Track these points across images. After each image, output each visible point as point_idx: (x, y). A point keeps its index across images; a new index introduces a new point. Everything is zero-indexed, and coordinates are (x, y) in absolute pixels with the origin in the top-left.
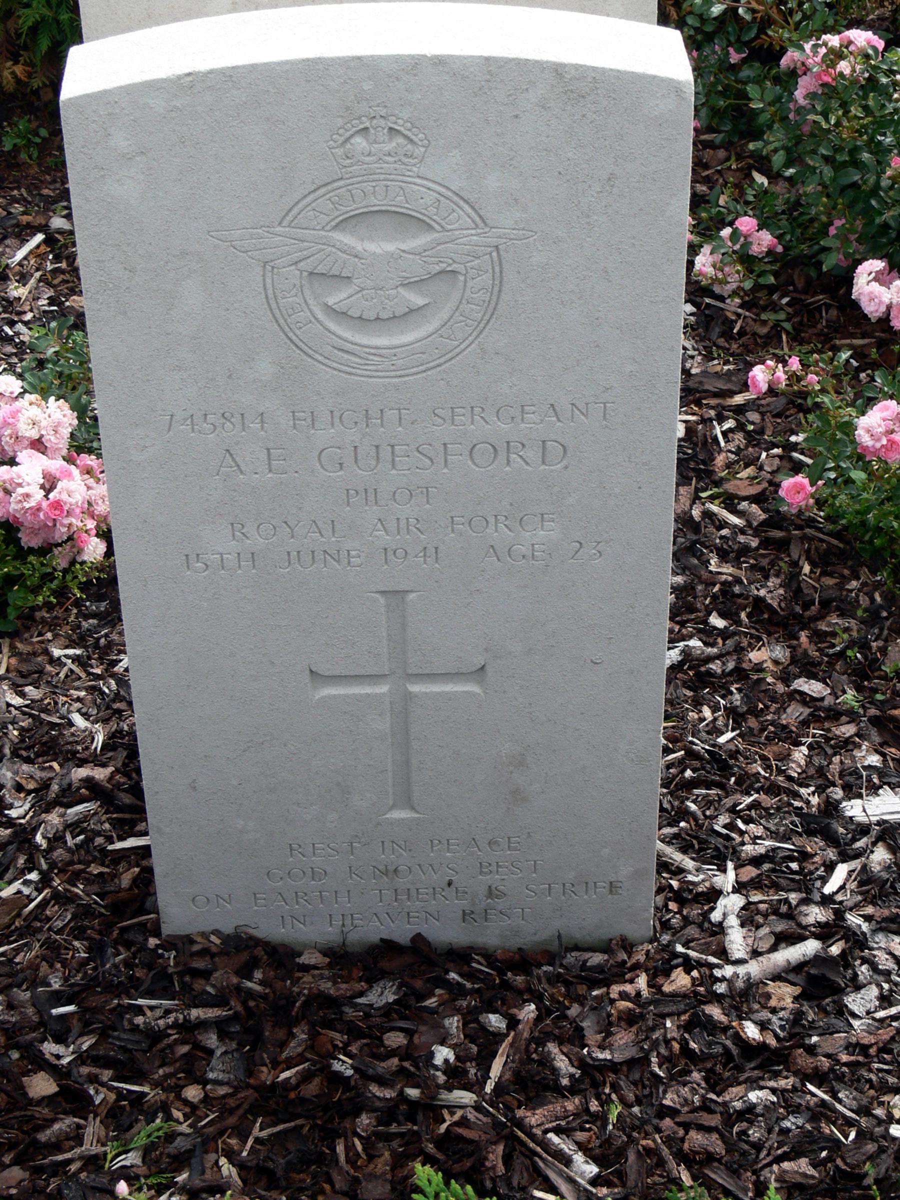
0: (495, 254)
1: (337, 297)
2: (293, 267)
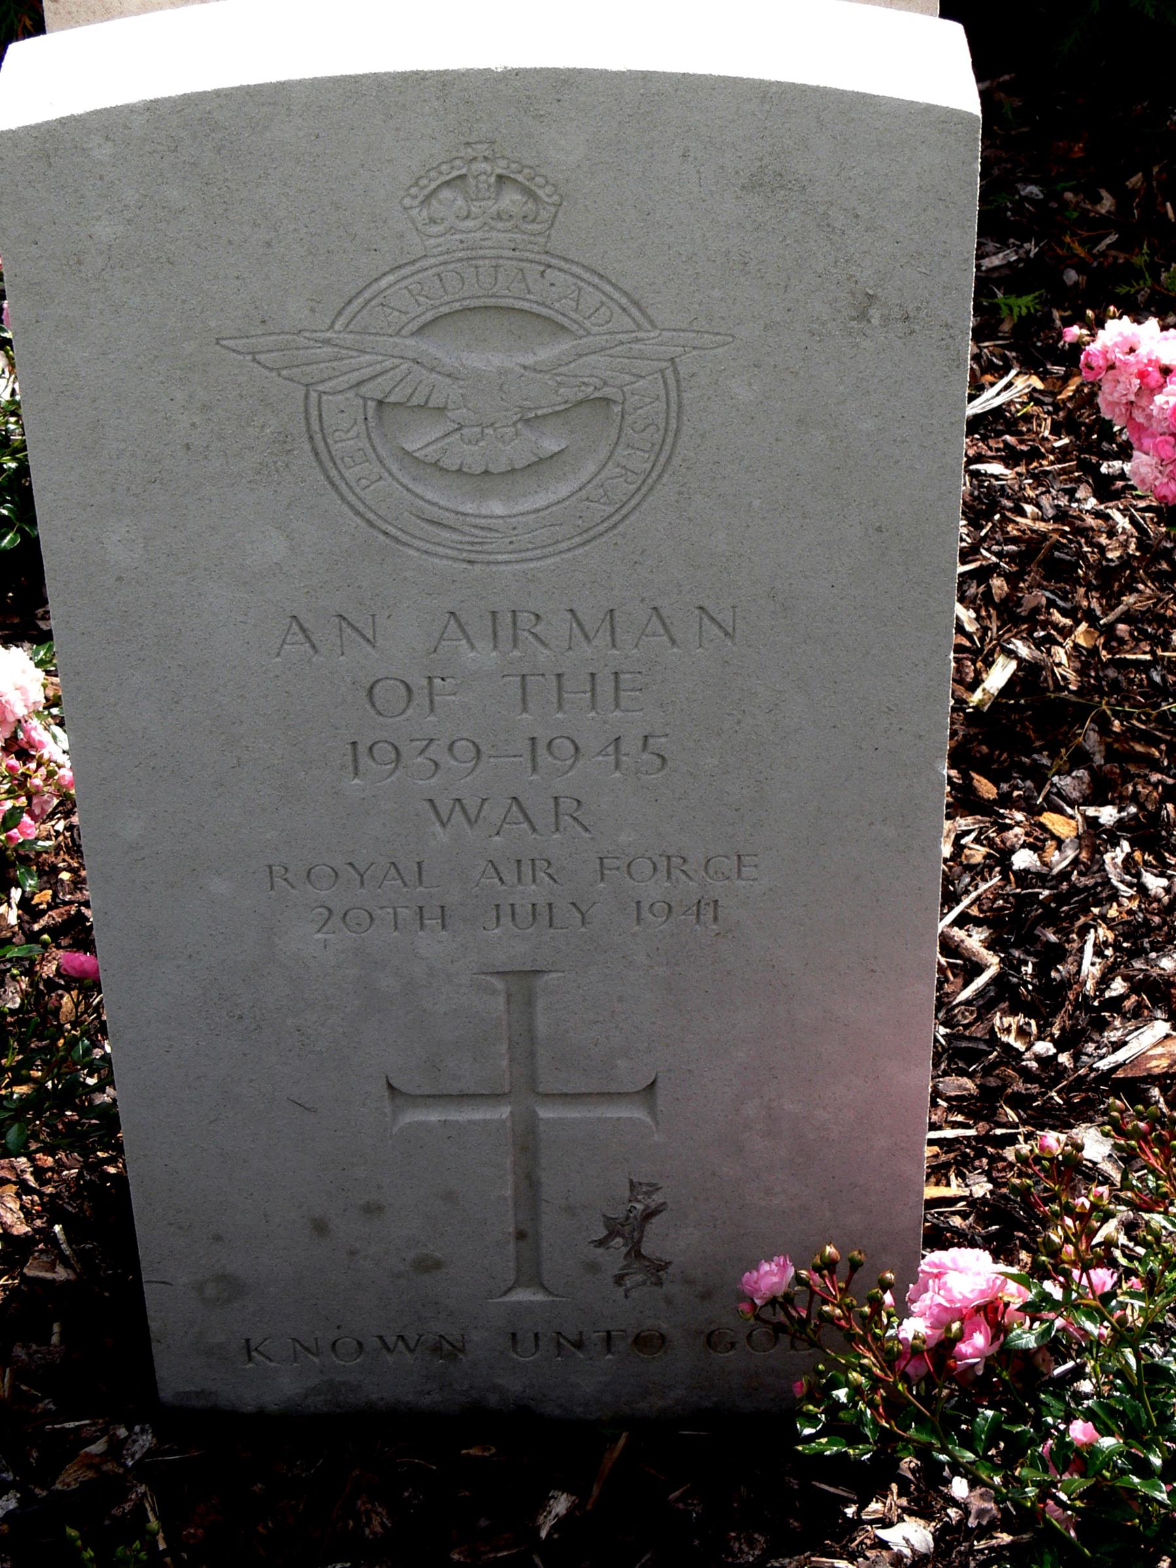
0: (669, 373)
1: (420, 439)
2: (350, 394)
